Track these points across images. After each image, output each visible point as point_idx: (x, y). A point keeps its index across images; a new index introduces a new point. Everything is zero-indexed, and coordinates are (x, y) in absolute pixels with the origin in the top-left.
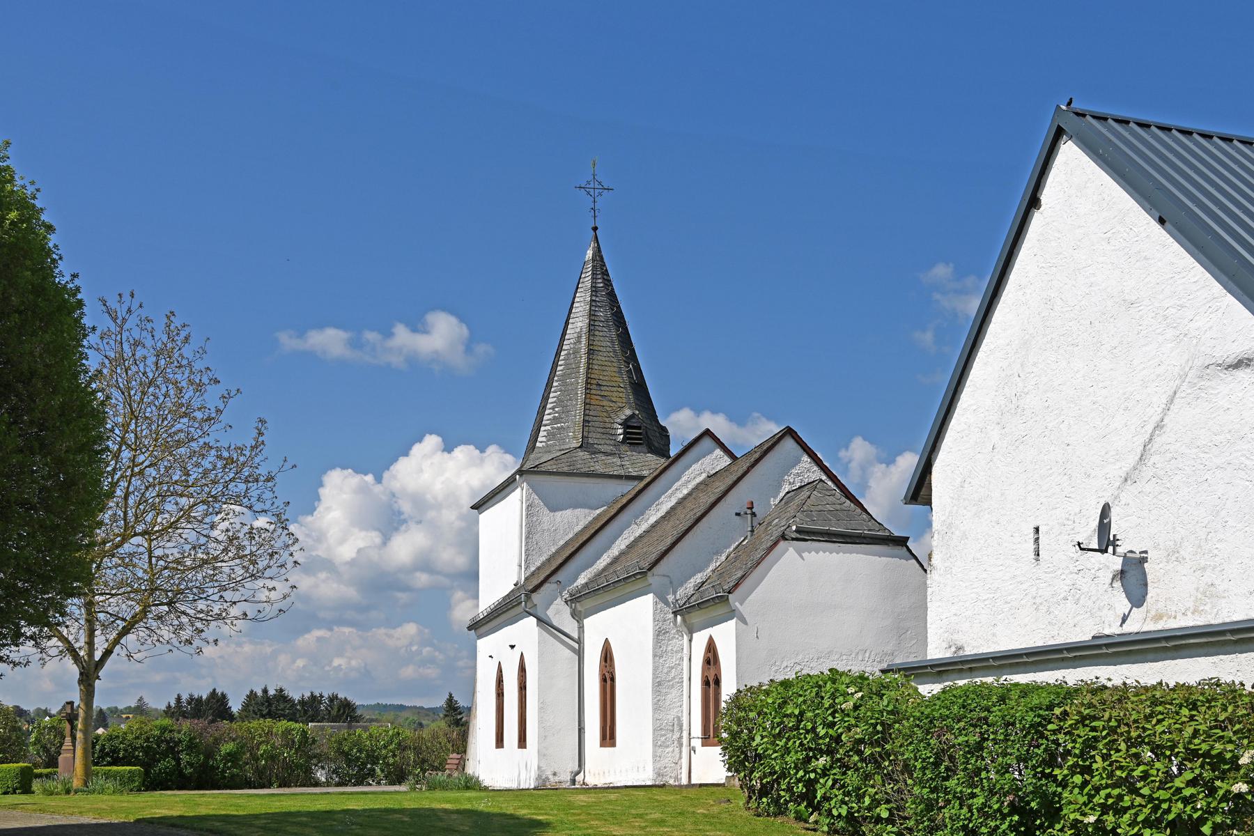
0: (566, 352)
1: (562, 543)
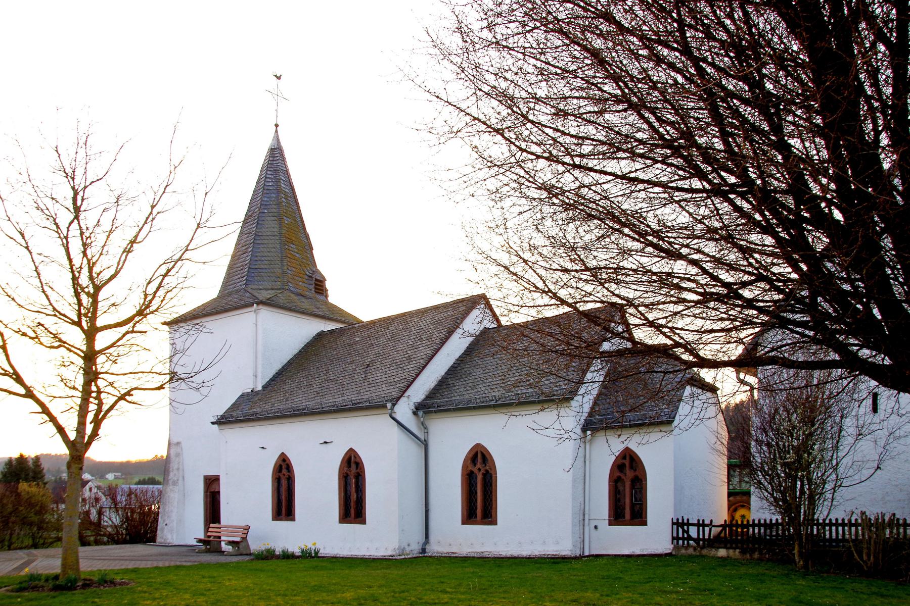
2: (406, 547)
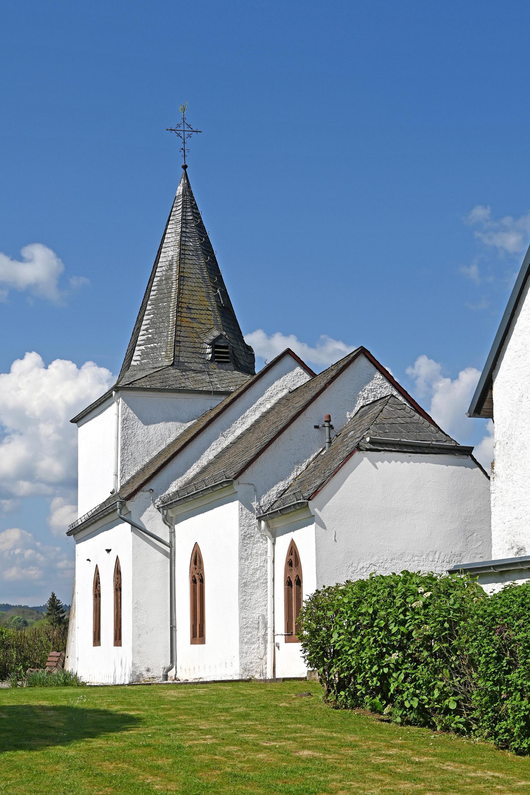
0: (159, 278)
1: (155, 453)
2: (144, 673)
